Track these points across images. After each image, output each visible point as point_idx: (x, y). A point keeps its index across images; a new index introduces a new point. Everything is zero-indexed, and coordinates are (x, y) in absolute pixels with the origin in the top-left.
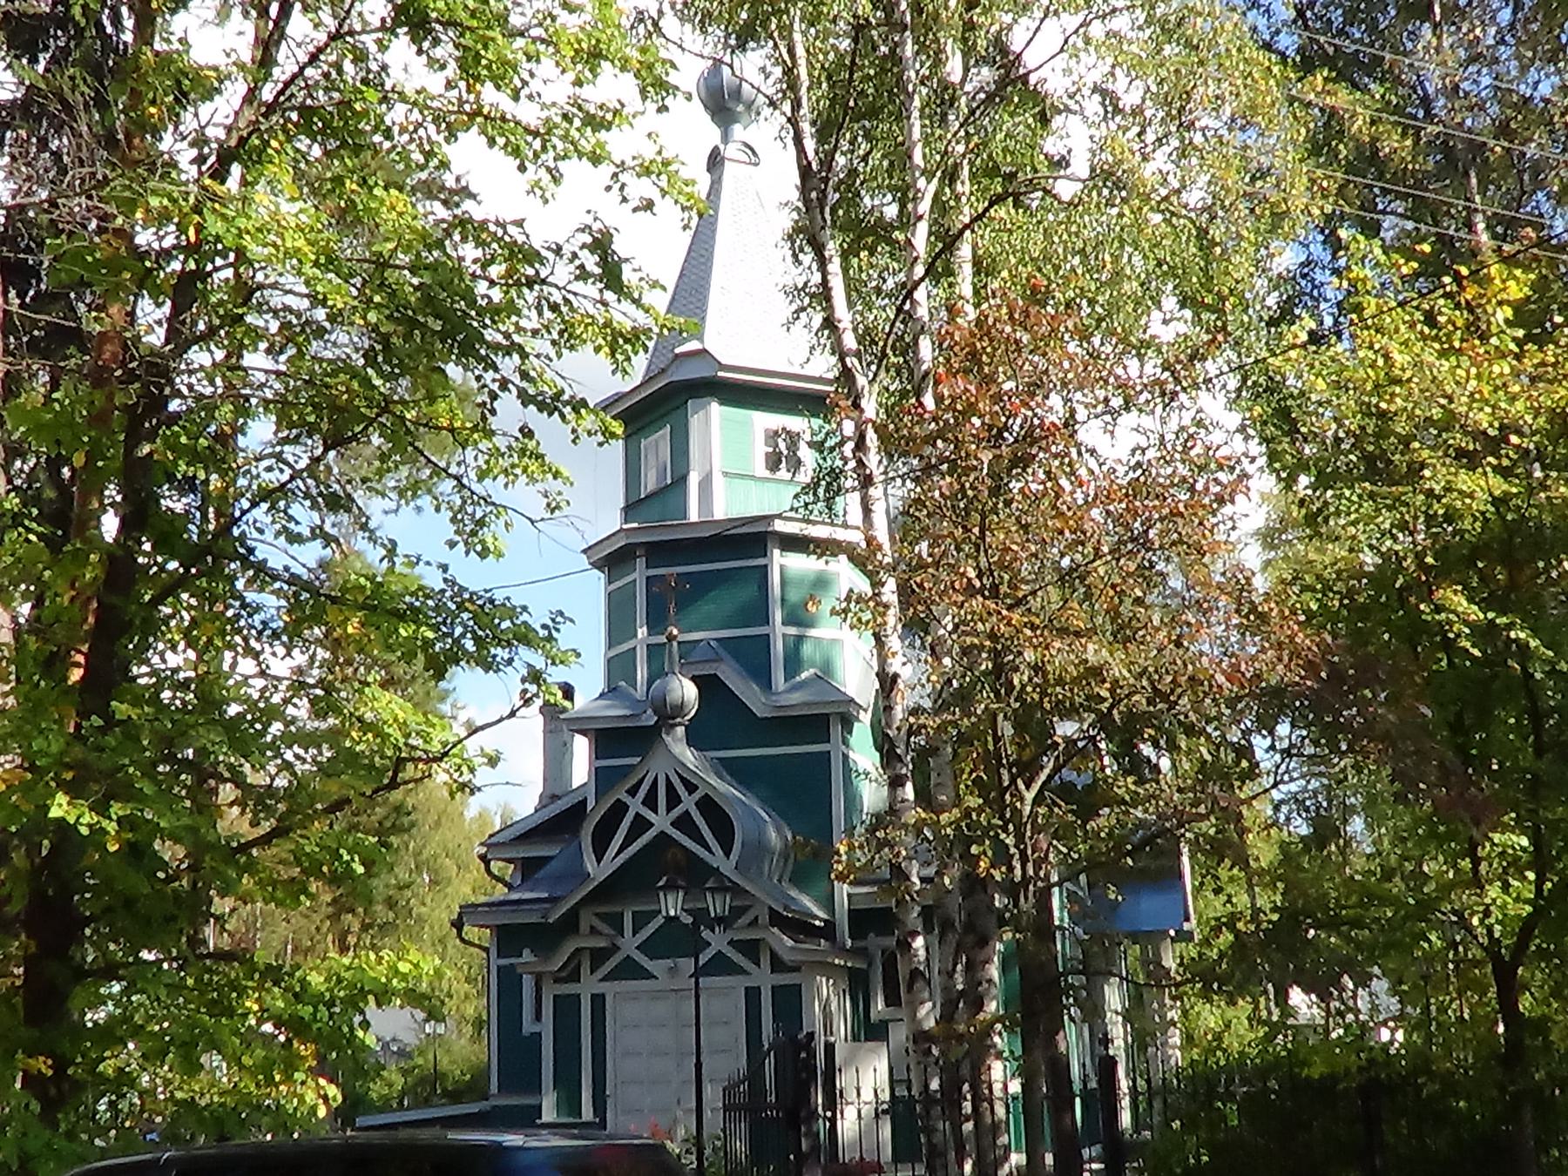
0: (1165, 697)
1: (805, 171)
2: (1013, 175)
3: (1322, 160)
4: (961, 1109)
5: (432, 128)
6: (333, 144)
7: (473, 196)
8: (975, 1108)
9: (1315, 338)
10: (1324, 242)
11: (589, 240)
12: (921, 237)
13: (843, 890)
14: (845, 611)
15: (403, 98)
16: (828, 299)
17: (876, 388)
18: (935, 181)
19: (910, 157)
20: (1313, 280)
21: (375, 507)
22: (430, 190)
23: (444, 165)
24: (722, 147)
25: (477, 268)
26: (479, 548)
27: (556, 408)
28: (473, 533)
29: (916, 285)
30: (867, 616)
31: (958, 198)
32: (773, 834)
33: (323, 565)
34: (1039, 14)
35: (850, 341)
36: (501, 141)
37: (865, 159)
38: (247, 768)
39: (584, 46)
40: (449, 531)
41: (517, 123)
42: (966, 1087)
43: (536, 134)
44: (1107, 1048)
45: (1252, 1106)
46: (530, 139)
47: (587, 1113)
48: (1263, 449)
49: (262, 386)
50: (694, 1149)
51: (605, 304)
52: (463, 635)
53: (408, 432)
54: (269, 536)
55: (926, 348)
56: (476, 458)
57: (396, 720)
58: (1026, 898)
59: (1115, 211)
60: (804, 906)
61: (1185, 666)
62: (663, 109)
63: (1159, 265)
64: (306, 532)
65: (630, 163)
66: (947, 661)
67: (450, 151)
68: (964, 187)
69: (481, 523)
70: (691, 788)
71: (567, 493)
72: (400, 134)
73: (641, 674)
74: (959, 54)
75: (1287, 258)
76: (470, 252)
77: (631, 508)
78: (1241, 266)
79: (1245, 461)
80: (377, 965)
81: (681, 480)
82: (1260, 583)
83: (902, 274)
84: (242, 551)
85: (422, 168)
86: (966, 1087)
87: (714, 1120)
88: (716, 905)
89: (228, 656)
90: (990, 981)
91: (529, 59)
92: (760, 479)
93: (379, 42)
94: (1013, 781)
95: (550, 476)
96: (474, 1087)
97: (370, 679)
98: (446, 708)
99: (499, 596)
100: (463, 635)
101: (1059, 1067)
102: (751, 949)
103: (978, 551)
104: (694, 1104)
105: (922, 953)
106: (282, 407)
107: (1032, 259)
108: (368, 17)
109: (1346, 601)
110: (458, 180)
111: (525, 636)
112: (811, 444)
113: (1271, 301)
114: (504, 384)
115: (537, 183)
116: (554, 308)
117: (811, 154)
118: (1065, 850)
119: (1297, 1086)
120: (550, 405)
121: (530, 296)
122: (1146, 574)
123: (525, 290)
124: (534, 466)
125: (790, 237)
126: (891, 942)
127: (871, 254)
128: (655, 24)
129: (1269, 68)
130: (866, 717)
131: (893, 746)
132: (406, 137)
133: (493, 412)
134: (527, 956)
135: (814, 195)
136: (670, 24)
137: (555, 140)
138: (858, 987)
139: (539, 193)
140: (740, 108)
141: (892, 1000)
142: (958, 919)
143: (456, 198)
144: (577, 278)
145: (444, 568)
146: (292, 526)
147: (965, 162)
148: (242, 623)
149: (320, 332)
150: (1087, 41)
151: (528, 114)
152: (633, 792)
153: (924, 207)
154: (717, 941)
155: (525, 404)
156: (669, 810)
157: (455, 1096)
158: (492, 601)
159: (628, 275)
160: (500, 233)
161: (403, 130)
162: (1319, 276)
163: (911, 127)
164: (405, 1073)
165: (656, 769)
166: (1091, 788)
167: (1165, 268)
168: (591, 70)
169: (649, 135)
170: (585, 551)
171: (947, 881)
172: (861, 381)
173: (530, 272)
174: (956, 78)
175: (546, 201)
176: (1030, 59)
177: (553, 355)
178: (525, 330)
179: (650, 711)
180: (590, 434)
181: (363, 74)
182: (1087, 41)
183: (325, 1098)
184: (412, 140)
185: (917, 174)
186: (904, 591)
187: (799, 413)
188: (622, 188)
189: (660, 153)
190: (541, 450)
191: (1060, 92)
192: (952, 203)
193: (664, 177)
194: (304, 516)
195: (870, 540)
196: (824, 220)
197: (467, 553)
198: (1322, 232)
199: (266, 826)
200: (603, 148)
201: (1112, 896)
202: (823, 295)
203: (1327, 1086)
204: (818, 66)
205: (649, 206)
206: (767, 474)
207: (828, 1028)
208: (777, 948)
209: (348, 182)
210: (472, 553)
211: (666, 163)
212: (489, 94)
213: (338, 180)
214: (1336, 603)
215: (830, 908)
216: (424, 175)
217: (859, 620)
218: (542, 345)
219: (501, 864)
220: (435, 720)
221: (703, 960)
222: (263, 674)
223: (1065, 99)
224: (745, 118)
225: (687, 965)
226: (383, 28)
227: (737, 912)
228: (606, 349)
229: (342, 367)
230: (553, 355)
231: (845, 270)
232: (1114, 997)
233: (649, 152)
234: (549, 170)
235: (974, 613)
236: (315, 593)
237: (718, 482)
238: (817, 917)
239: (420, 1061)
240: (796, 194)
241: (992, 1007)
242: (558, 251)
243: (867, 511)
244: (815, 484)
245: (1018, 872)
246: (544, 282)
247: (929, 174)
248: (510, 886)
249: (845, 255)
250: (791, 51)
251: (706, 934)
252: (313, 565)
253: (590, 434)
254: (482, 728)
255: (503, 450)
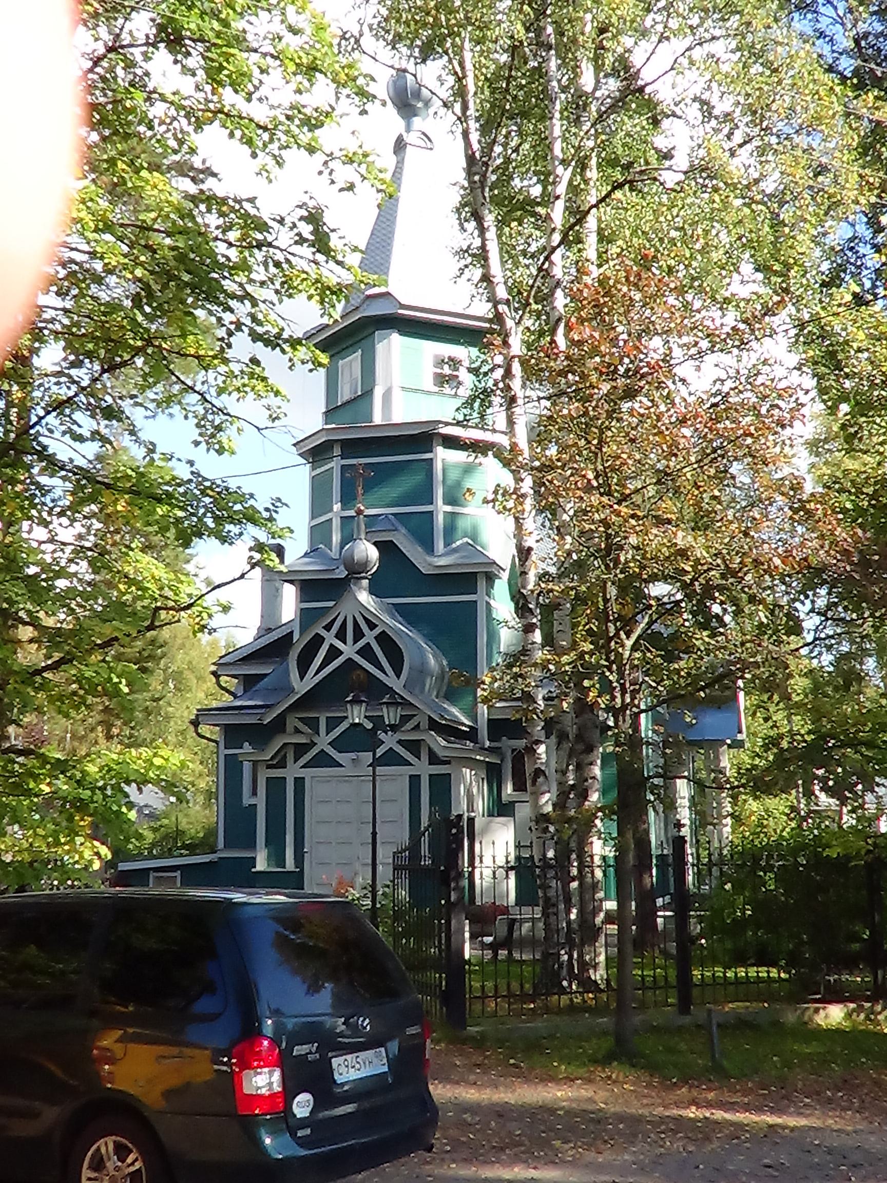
0: (734, 574)
1: (471, 159)
2: (630, 165)
3: (868, 158)
4: (569, 872)
5: (184, 122)
6: (107, 132)
7: (214, 175)
8: (580, 871)
9: (859, 300)
10: (867, 223)
11: (306, 214)
12: (558, 214)
13: (483, 709)
14: (493, 501)
15: (163, 98)
16: (486, 259)
17: (521, 328)
18: (570, 169)
19: (552, 150)
20: (857, 252)
21: (137, 415)
22: (183, 169)
23: (193, 151)
24: (405, 135)
25: (218, 233)
26: (217, 447)
27: (278, 345)
28: (213, 436)
29: (554, 249)
30: (510, 504)
31: (586, 182)
32: (432, 661)
33: (99, 458)
34: (655, 39)
35: (501, 292)
36: (238, 133)
37: (516, 150)
38: (41, 614)
39: (305, 61)
40: (195, 434)
41: (251, 120)
42: (574, 856)
43: (265, 129)
44: (679, 831)
45: (785, 876)
46: (260, 132)
47: (290, 864)
48: (814, 382)
49: (52, 321)
50: (369, 895)
51: (316, 262)
52: (204, 515)
53: (165, 358)
54: (57, 435)
55: (560, 300)
56: (216, 379)
57: (153, 577)
58: (624, 721)
59: (706, 196)
60: (456, 717)
61: (751, 549)
62: (364, 112)
63: (740, 238)
64: (87, 434)
65: (337, 154)
66: (569, 539)
67: (196, 139)
68: (592, 174)
69: (219, 428)
70: (372, 626)
71: (285, 407)
72: (160, 125)
73: (336, 538)
74: (592, 69)
75: (839, 233)
76: (213, 220)
77: (330, 413)
78: (803, 243)
79: (800, 394)
80: (137, 757)
81: (368, 393)
82: (809, 487)
83: (543, 240)
84: (39, 448)
85: (175, 152)
86: (574, 856)
87: (385, 872)
88: (390, 716)
89: (26, 525)
90: (594, 778)
91: (262, 71)
92: (429, 393)
93: (145, 54)
94: (617, 634)
95: (272, 394)
96: (206, 844)
97: (133, 545)
98: (190, 568)
99: (233, 484)
100: (204, 515)
101: (643, 843)
102: (414, 747)
103: (596, 458)
104: (370, 861)
105: (544, 756)
106: (70, 337)
107: (643, 232)
108: (135, 34)
109: (873, 502)
110: (204, 162)
111: (251, 517)
112: (470, 370)
113: (825, 266)
114: (239, 325)
115: (264, 168)
116: (277, 265)
117: (476, 146)
118: (654, 684)
119: (818, 862)
120: (272, 342)
121: (259, 255)
122: (723, 475)
123: (256, 251)
124: (260, 386)
125: (458, 210)
126: (521, 743)
127: (520, 225)
128: (357, 41)
129: (831, 88)
130: (505, 576)
131: (527, 602)
132: (164, 128)
133: (229, 346)
134: (247, 747)
135: (477, 178)
136: (368, 42)
137: (280, 134)
138: (493, 775)
139: (265, 174)
140: (420, 105)
141: (520, 786)
142: (572, 731)
143: (201, 176)
144: (296, 243)
145: (191, 463)
146: (75, 427)
147: (594, 154)
148: (37, 500)
149: (98, 280)
150: (692, 63)
151: (259, 112)
152: (328, 628)
153: (561, 189)
154: (389, 741)
155: (254, 341)
156: (355, 642)
157: (192, 849)
158: (227, 489)
159: (334, 242)
160: (237, 207)
161: (162, 123)
162: (864, 249)
163: (553, 126)
164: (155, 830)
165: (345, 611)
166: (675, 636)
167: (744, 240)
168: (309, 80)
169: (353, 133)
170: (294, 445)
171: (565, 705)
172: (510, 323)
173: (259, 236)
174: (589, 88)
175: (270, 181)
176: (646, 76)
177: (276, 301)
178: (254, 281)
179: (342, 568)
180: (303, 363)
181: (131, 77)
182: (692, 63)
183: (97, 854)
184: (168, 130)
185: (557, 163)
186: (538, 484)
187: (458, 343)
188: (330, 174)
189: (361, 147)
190: (266, 374)
191: (669, 101)
192: (582, 186)
193: (364, 166)
194: (86, 423)
195: (514, 447)
196: (484, 198)
197: (208, 450)
198: (866, 215)
199: (57, 656)
200: (317, 142)
201: (688, 720)
202: (482, 256)
203: (841, 865)
204: (483, 78)
205: (351, 187)
206: (436, 389)
207: (471, 808)
208: (432, 746)
209: (119, 163)
210: (212, 451)
211: (365, 155)
212: (229, 96)
213: (112, 162)
214: (866, 503)
215: (474, 719)
216: (177, 158)
217: (504, 508)
218: (267, 294)
219: (228, 679)
220: (183, 578)
221: (380, 752)
222: (51, 541)
223: (673, 107)
224: (423, 113)
225: (368, 757)
226: (147, 44)
227: (405, 719)
228: (317, 298)
229: (113, 307)
230: (276, 301)
231: (499, 237)
232: (683, 788)
233: (352, 147)
234: (275, 156)
235: (592, 506)
236: (92, 480)
237: (397, 394)
238: (463, 724)
239: (166, 821)
240: (464, 175)
241: (594, 797)
242: (281, 221)
243: (511, 422)
244: (473, 399)
245: (618, 700)
246: (270, 245)
247: (564, 162)
248: (235, 696)
249: (502, 223)
250: (462, 64)
251: (382, 736)
252: (91, 458)
253: (303, 363)
254: (219, 586)
255: (237, 373)
